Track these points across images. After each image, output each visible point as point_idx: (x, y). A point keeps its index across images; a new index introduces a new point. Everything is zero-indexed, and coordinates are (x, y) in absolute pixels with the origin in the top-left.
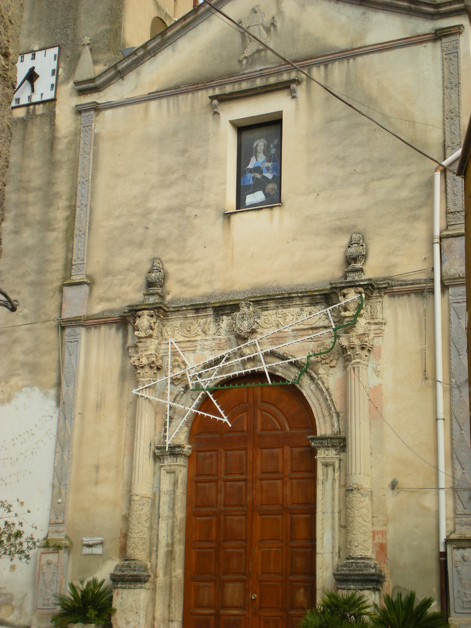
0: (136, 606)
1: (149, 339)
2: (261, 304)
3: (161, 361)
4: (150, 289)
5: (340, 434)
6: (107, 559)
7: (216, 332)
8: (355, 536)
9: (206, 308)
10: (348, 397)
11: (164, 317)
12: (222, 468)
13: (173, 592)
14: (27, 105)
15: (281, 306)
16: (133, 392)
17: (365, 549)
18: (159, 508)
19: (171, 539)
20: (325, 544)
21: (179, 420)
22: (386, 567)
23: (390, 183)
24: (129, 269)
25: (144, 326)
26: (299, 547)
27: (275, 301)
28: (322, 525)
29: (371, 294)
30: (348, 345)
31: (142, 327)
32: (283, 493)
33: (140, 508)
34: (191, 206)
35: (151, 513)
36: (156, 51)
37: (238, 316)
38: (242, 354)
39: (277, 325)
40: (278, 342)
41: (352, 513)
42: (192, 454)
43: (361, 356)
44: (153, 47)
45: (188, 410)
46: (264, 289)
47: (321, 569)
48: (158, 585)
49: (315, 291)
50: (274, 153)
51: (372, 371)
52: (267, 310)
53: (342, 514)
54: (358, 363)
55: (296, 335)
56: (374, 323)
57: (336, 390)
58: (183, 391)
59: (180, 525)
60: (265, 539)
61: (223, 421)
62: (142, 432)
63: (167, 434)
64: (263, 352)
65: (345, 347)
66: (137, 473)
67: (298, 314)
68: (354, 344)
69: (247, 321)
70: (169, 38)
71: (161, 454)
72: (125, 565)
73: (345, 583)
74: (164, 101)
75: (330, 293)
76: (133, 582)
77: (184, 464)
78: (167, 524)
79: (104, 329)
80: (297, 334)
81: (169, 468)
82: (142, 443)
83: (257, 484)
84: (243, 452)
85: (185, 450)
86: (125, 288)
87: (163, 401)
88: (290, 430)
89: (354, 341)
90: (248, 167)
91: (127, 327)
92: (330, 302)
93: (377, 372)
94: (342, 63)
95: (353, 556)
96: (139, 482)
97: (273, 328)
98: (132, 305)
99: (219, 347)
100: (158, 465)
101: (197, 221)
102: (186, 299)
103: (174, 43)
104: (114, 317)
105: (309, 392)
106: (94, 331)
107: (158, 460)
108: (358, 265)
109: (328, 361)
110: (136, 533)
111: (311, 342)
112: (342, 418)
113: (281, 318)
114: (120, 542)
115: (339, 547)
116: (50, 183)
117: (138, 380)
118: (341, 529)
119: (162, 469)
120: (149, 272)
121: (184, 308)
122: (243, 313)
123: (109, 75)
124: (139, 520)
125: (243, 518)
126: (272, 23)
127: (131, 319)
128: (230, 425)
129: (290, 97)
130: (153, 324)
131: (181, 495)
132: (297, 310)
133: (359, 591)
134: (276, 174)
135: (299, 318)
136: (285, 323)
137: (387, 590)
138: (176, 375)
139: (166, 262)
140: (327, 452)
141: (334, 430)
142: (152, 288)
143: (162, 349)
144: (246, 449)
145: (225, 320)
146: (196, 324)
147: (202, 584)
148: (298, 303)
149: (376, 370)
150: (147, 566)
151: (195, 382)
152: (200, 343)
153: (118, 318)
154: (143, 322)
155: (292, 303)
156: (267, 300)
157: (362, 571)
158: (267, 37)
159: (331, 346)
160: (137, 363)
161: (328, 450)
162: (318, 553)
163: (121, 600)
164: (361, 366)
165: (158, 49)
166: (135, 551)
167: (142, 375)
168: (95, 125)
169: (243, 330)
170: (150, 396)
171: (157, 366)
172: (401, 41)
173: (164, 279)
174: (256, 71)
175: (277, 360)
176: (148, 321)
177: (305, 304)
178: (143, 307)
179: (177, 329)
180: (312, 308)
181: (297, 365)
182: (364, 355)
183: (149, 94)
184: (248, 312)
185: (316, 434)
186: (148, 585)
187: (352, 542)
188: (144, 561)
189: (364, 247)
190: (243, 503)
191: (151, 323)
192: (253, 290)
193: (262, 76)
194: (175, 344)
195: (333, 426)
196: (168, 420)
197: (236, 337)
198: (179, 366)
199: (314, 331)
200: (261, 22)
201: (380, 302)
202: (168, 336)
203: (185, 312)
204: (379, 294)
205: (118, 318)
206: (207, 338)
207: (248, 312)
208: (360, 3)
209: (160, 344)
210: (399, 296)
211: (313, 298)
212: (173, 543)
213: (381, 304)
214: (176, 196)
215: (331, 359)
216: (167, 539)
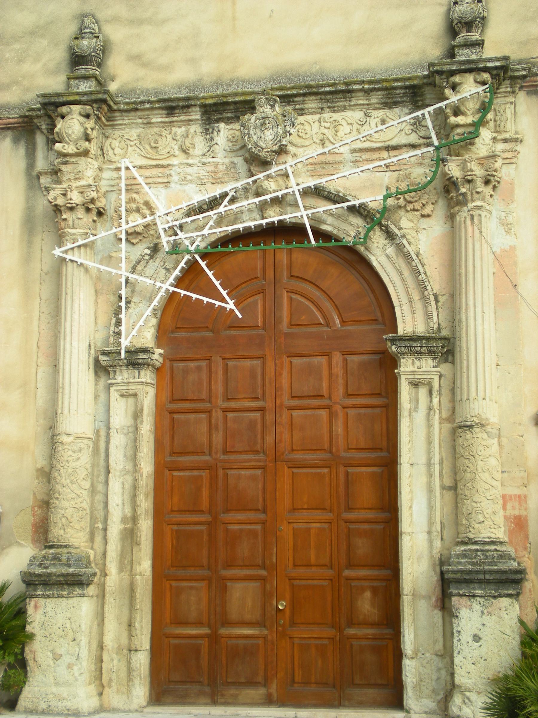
0: (72, 629)
1: (83, 159)
2: (293, 102)
3: (104, 200)
4: (80, 67)
5: (440, 332)
6: (10, 545)
7: (206, 150)
8: (478, 505)
9: (188, 107)
10: (460, 266)
11: (107, 121)
12: (219, 388)
13: (138, 601)
15: (329, 107)
16: (54, 252)
17: (496, 527)
18: (107, 456)
19: (130, 510)
20: (414, 516)
21: (141, 305)
22: (527, 556)
25: (73, 133)
26: (361, 522)
27: (319, 97)
28: (410, 486)
30: (462, 177)
31: (70, 135)
32: (331, 431)
33: (75, 455)
35: (93, 466)
37: (252, 121)
38: (260, 190)
39: (321, 140)
40: (323, 172)
41: (470, 465)
42: (163, 364)
43: (485, 196)
45: (161, 288)
47: (409, 559)
48: (107, 589)
49: (396, 80)
51: (499, 224)
52: (302, 115)
53: (444, 466)
54: (479, 208)
55: (358, 158)
56: (502, 140)
57: (433, 256)
58: (149, 255)
59: (147, 486)
60: (300, 507)
61: (226, 308)
62: (75, 324)
63: (123, 328)
64: (301, 187)
66: (67, 396)
67: (361, 123)
68: (474, 173)
69: (271, 131)
71: (111, 363)
72: (50, 556)
73: (464, 585)
75: (424, 84)
76: (66, 587)
77: (152, 382)
78: (123, 484)
80: (361, 157)
81: (125, 388)
82: (75, 344)
83: (284, 417)
84: (257, 363)
85: (156, 356)
86: (27, 67)
87: (114, 271)
88: (341, 326)
89: (473, 169)
91: (34, 138)
92: (419, 101)
95: (476, 539)
96: (71, 411)
97: (314, 146)
98: (50, 94)
99: (213, 178)
100: (102, 382)
102: (148, 90)
104: (10, 118)
105: (383, 259)
107: (102, 374)
108: (475, 36)
109: (417, 206)
110: (68, 501)
111: (386, 171)
112: (443, 305)
113: (328, 128)
114: (34, 515)
115: (441, 523)
117: (64, 232)
118: (444, 492)
119: (112, 389)
120: (76, 38)
121: (147, 106)
122: (263, 116)
124: (73, 477)
125: (259, 472)
127: (43, 123)
128: (240, 316)
130: (90, 130)
131: (148, 433)
132: (358, 115)
133: (491, 599)
135: (362, 129)
136: (337, 138)
137: (531, 595)
138: (135, 226)
139: (106, 21)
140: (417, 363)
141: (431, 324)
142: (83, 67)
143: (105, 179)
144: (262, 357)
145: (222, 131)
146: (168, 136)
147: (185, 584)
148: (361, 102)
149: (505, 222)
150: (90, 556)
151: (173, 238)
152: (179, 170)
153: (16, 120)
154: (70, 127)
155: (350, 101)
156: (304, 95)
157: (496, 565)
159: (429, 178)
160: (60, 201)
161: (419, 359)
162: (404, 533)
163: (43, 617)
164: (483, 214)
166: (66, 530)
167: (70, 223)
169: (264, 146)
170: (87, 260)
171: (97, 208)
173: (103, 52)
175: (324, 202)
176: (82, 124)
177: (374, 104)
178: (71, 98)
179: (132, 143)
180: (387, 111)
181: (362, 211)
184: (272, 114)
185: (396, 332)
186: (91, 590)
187: (473, 515)
188: (83, 548)
190: (258, 447)
191: (86, 128)
192: (275, 77)
194: (134, 170)
195: (428, 316)
196: (123, 304)
197: (246, 160)
198: (138, 210)
199: (392, 153)
201: (511, 103)
202: (113, 156)
203: (147, 113)
204: (511, 87)
205: (16, 120)
206: (190, 161)
207: (272, 114)
209: (100, 169)
212: (135, 516)
213: (513, 106)
215: (424, 203)
216: (123, 509)
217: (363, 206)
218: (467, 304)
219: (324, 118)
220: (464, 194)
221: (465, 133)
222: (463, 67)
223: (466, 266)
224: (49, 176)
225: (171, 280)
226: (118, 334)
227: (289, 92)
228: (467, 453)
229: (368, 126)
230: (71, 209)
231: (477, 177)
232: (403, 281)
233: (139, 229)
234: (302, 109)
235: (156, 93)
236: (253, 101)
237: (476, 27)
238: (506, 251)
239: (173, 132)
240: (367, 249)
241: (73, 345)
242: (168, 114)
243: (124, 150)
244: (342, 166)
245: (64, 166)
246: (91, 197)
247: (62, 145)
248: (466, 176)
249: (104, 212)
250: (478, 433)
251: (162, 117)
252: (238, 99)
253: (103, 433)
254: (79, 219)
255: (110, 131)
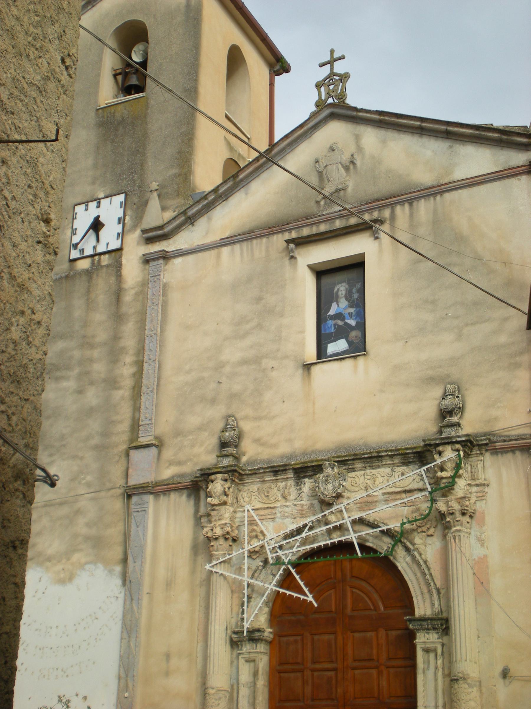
1: (224, 507)
3: (236, 532)
5: (442, 614)
9: (286, 470)
12: (309, 654)
14: (92, 256)
15: (369, 466)
16: (206, 567)
23: (487, 327)
24: (201, 428)
25: (217, 491)
27: (362, 460)
29: (471, 452)
31: (215, 493)
32: (379, 684)
33: (217, 702)
34: (267, 358)
36: (227, 194)
37: (321, 478)
39: (365, 487)
40: (366, 508)
44: (225, 190)
45: (268, 588)
46: (350, 448)
49: (407, 449)
50: (356, 297)
52: (354, 471)
54: (459, 531)
57: (436, 562)
58: (262, 566)
61: (307, 600)
62: (217, 614)
63: (245, 616)
65: (443, 512)
66: (212, 662)
67: (389, 476)
68: (453, 508)
69: (331, 484)
70: (242, 180)
74: (237, 247)
79: (173, 496)
80: (389, 498)
82: (217, 627)
84: (332, 636)
85: (266, 634)
87: (240, 578)
88: (385, 610)
89: (453, 506)
90: (329, 314)
93: (481, 542)
94: (429, 200)
97: (361, 491)
99: (301, 514)
100: (236, 652)
101: (274, 374)
103: (247, 186)
105: (404, 565)
106: (163, 499)
109: (424, 529)
111: (405, 507)
112: (443, 596)
113: (369, 479)
116: (116, 337)
119: (240, 657)
121: (261, 471)
123: (178, 222)
126: (351, 161)
128: (316, 605)
129: (373, 238)
132: (388, 470)
134: (360, 321)
140: (427, 636)
144: (335, 633)
145: (307, 484)
148: (388, 462)
152: (280, 510)
155: (382, 462)
156: (353, 460)
158: (346, 176)
160: (209, 535)
161: (428, 633)
164: (462, 534)
165: (230, 193)
167: (215, 548)
168: (164, 274)
169: (327, 494)
171: (232, 537)
172: (492, 175)
174: (335, 212)
176: (222, 486)
177: (396, 463)
178: (216, 470)
179: (254, 494)
180: (405, 468)
181: (389, 533)
182: (466, 521)
183: (221, 239)
189: (460, 398)
192: (338, 449)
193: (341, 217)
195: (433, 605)
196: (245, 599)
198: (256, 537)
199: (408, 495)
200: (339, 160)
201: (481, 460)
203: (262, 475)
204: (479, 451)
206: (287, 504)
207: (332, 473)
208: (446, 136)
209: (235, 512)
210: (502, 453)
211: (404, 457)
214: (251, 347)
215: (428, 527)
217: (389, 530)
218: (453, 596)
219: (367, 474)
220: (449, 522)
221: (446, 483)
222: (442, 442)
223: (452, 570)
224: (206, 518)
225: (274, 582)
226: (243, 619)
227: (343, 459)
228: (455, 698)
229: (394, 478)
230: (216, 539)
231: (456, 511)
232: (417, 579)
233: (257, 549)
234: (353, 468)
235: (269, 462)
236: (321, 465)
237: (455, 413)
238: (481, 559)
239: (278, 486)
240: (394, 558)
241: (216, 628)
242: (274, 475)
243: (249, 499)
244: (378, 504)
245: (213, 512)
246: (227, 531)
247: (211, 499)
248: (449, 510)
249: (237, 539)
250: (462, 684)
251: (271, 477)
252: (314, 464)
253: (235, 687)
254: (221, 545)
255: (242, 487)
